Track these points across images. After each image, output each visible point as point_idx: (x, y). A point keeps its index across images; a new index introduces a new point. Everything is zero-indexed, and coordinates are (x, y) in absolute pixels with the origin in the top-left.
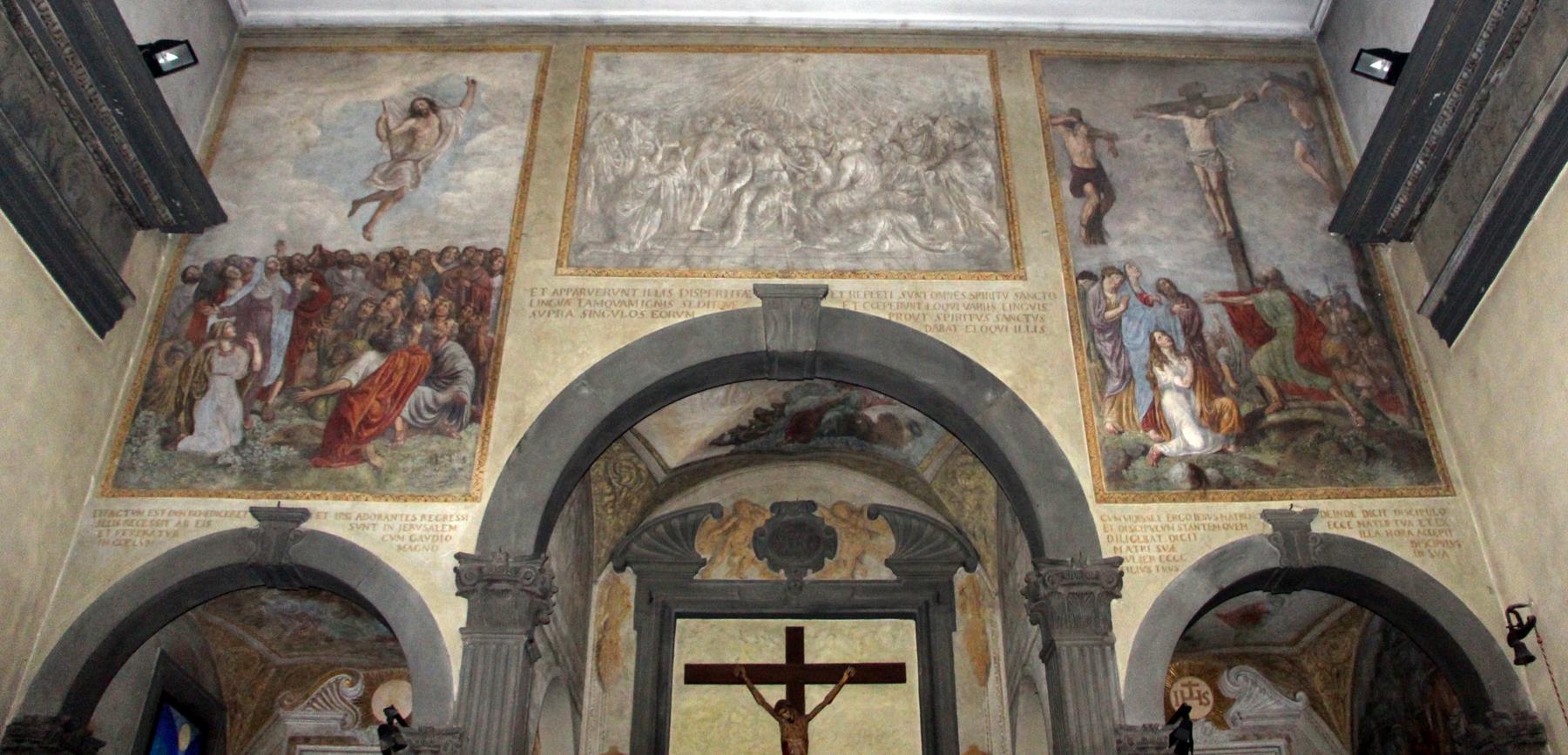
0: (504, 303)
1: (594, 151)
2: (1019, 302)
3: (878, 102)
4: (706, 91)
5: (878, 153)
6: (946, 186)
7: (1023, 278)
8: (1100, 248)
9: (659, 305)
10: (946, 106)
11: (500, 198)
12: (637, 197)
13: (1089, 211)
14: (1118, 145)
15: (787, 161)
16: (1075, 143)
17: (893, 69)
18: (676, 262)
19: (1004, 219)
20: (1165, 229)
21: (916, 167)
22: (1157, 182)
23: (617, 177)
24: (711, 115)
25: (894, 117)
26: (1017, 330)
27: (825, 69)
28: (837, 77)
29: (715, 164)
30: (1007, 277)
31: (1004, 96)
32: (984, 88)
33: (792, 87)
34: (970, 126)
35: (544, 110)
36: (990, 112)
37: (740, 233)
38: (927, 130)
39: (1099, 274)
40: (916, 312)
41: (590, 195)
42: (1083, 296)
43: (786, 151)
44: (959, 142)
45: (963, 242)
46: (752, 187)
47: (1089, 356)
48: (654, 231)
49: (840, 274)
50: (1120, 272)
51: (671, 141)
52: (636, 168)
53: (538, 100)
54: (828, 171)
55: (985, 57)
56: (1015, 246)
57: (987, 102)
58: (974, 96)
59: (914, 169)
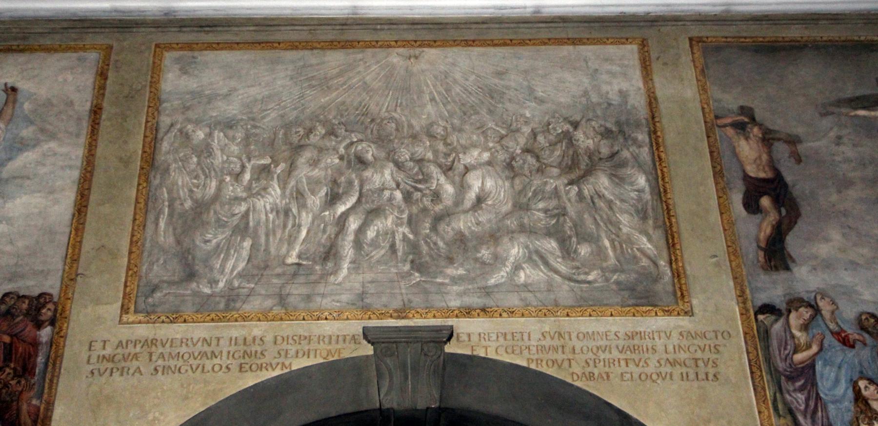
0: (54, 361)
1: (167, 170)
2: (685, 343)
3: (508, 105)
4: (302, 97)
5: (509, 166)
6: (591, 203)
7: (689, 313)
8: (783, 275)
9: (248, 355)
10: (590, 107)
11: (51, 232)
12: (221, 224)
13: (767, 230)
14: (801, 148)
15: (400, 177)
16: (748, 151)
17: (524, 64)
18: (269, 303)
19: (662, 243)
20: (865, 251)
21: (555, 181)
22: (853, 193)
23: (196, 201)
24: (308, 124)
25: (527, 123)
26: (684, 377)
27: (442, 68)
28: (458, 76)
29: (314, 184)
30: (669, 313)
31: (659, 94)
32: (634, 84)
33: (406, 90)
34: (618, 131)
35: (105, 123)
36: (643, 113)
37: (346, 265)
38: (567, 137)
39: (783, 307)
40: (559, 356)
41: (162, 224)
42: (765, 334)
43: (399, 166)
44: (605, 151)
45: (615, 271)
46: (360, 209)
47: (776, 409)
48: (241, 265)
49: (467, 312)
50: (809, 305)
51: (261, 156)
52: (219, 189)
53: (96, 111)
54: (449, 189)
55: (635, 47)
56: (677, 275)
57: (638, 101)
58: (622, 94)
59: (552, 184)
